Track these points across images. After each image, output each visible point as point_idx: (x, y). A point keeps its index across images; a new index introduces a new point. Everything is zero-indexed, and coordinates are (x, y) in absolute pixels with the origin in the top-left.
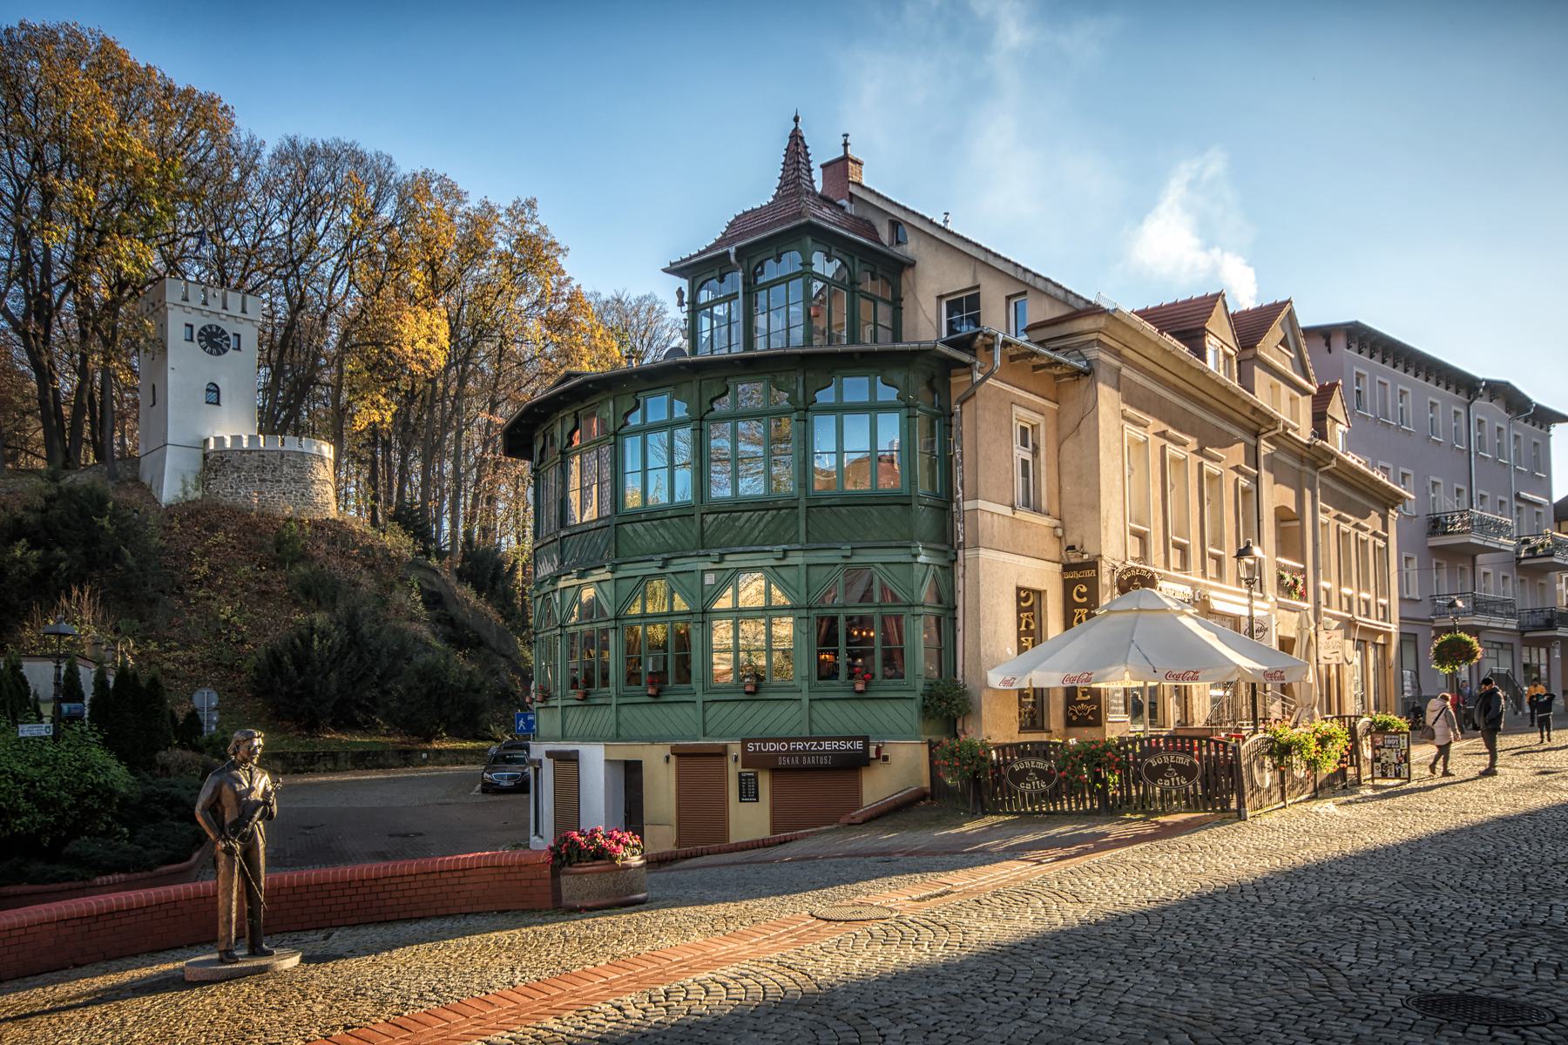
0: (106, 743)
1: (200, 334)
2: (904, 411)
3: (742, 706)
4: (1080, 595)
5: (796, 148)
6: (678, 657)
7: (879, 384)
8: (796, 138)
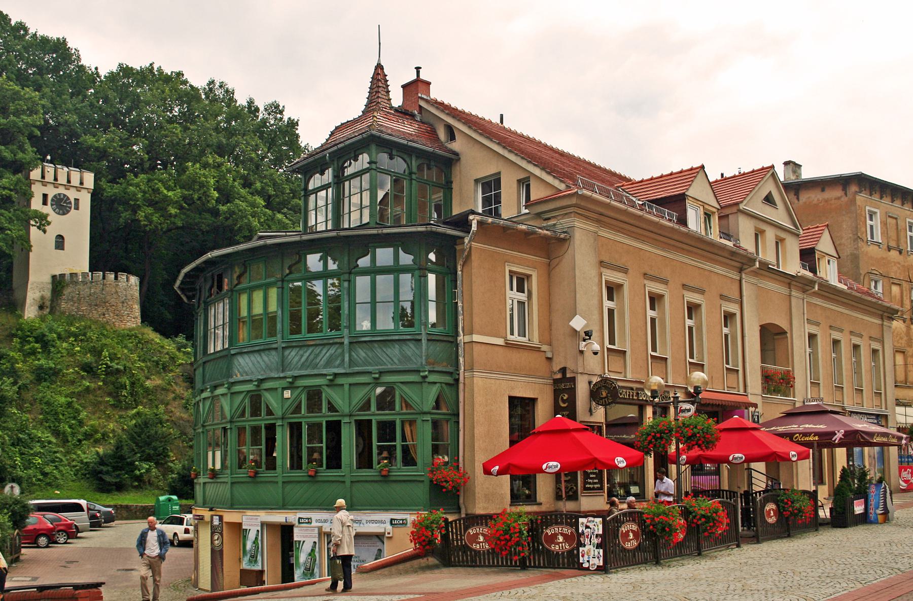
0: (831, 509)
1: (52, 200)
2: (417, 273)
3: (306, 486)
4: (564, 401)
5: (379, 79)
6: (403, 446)
7: (401, 251)
8: (379, 67)
